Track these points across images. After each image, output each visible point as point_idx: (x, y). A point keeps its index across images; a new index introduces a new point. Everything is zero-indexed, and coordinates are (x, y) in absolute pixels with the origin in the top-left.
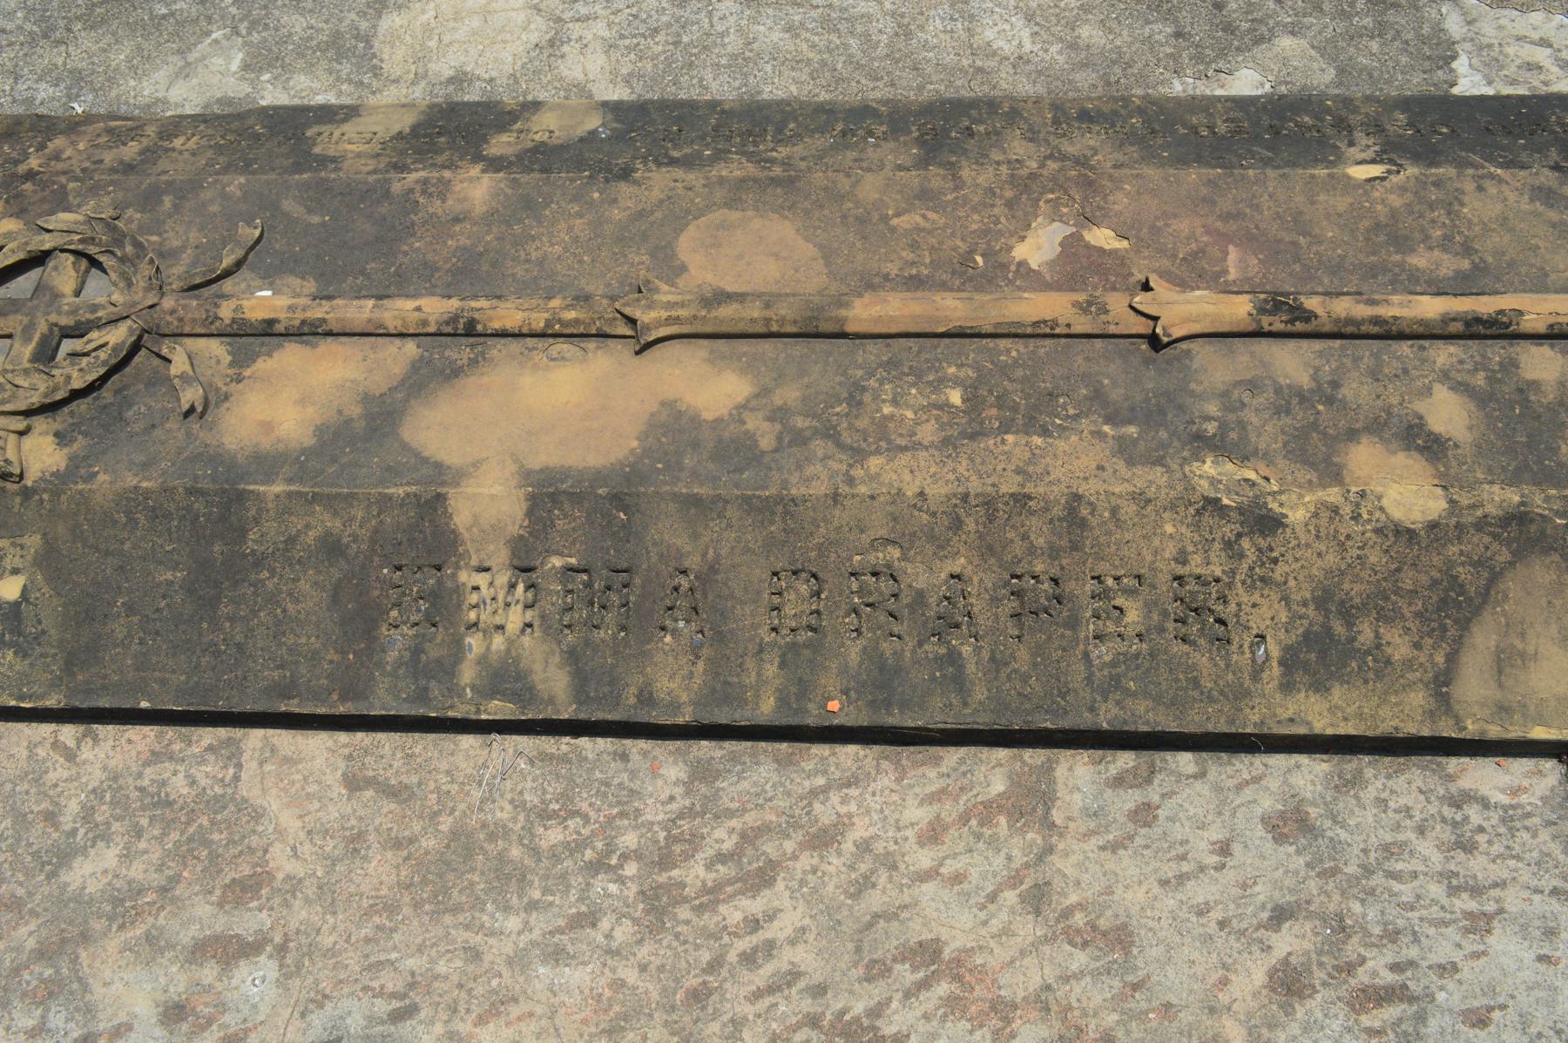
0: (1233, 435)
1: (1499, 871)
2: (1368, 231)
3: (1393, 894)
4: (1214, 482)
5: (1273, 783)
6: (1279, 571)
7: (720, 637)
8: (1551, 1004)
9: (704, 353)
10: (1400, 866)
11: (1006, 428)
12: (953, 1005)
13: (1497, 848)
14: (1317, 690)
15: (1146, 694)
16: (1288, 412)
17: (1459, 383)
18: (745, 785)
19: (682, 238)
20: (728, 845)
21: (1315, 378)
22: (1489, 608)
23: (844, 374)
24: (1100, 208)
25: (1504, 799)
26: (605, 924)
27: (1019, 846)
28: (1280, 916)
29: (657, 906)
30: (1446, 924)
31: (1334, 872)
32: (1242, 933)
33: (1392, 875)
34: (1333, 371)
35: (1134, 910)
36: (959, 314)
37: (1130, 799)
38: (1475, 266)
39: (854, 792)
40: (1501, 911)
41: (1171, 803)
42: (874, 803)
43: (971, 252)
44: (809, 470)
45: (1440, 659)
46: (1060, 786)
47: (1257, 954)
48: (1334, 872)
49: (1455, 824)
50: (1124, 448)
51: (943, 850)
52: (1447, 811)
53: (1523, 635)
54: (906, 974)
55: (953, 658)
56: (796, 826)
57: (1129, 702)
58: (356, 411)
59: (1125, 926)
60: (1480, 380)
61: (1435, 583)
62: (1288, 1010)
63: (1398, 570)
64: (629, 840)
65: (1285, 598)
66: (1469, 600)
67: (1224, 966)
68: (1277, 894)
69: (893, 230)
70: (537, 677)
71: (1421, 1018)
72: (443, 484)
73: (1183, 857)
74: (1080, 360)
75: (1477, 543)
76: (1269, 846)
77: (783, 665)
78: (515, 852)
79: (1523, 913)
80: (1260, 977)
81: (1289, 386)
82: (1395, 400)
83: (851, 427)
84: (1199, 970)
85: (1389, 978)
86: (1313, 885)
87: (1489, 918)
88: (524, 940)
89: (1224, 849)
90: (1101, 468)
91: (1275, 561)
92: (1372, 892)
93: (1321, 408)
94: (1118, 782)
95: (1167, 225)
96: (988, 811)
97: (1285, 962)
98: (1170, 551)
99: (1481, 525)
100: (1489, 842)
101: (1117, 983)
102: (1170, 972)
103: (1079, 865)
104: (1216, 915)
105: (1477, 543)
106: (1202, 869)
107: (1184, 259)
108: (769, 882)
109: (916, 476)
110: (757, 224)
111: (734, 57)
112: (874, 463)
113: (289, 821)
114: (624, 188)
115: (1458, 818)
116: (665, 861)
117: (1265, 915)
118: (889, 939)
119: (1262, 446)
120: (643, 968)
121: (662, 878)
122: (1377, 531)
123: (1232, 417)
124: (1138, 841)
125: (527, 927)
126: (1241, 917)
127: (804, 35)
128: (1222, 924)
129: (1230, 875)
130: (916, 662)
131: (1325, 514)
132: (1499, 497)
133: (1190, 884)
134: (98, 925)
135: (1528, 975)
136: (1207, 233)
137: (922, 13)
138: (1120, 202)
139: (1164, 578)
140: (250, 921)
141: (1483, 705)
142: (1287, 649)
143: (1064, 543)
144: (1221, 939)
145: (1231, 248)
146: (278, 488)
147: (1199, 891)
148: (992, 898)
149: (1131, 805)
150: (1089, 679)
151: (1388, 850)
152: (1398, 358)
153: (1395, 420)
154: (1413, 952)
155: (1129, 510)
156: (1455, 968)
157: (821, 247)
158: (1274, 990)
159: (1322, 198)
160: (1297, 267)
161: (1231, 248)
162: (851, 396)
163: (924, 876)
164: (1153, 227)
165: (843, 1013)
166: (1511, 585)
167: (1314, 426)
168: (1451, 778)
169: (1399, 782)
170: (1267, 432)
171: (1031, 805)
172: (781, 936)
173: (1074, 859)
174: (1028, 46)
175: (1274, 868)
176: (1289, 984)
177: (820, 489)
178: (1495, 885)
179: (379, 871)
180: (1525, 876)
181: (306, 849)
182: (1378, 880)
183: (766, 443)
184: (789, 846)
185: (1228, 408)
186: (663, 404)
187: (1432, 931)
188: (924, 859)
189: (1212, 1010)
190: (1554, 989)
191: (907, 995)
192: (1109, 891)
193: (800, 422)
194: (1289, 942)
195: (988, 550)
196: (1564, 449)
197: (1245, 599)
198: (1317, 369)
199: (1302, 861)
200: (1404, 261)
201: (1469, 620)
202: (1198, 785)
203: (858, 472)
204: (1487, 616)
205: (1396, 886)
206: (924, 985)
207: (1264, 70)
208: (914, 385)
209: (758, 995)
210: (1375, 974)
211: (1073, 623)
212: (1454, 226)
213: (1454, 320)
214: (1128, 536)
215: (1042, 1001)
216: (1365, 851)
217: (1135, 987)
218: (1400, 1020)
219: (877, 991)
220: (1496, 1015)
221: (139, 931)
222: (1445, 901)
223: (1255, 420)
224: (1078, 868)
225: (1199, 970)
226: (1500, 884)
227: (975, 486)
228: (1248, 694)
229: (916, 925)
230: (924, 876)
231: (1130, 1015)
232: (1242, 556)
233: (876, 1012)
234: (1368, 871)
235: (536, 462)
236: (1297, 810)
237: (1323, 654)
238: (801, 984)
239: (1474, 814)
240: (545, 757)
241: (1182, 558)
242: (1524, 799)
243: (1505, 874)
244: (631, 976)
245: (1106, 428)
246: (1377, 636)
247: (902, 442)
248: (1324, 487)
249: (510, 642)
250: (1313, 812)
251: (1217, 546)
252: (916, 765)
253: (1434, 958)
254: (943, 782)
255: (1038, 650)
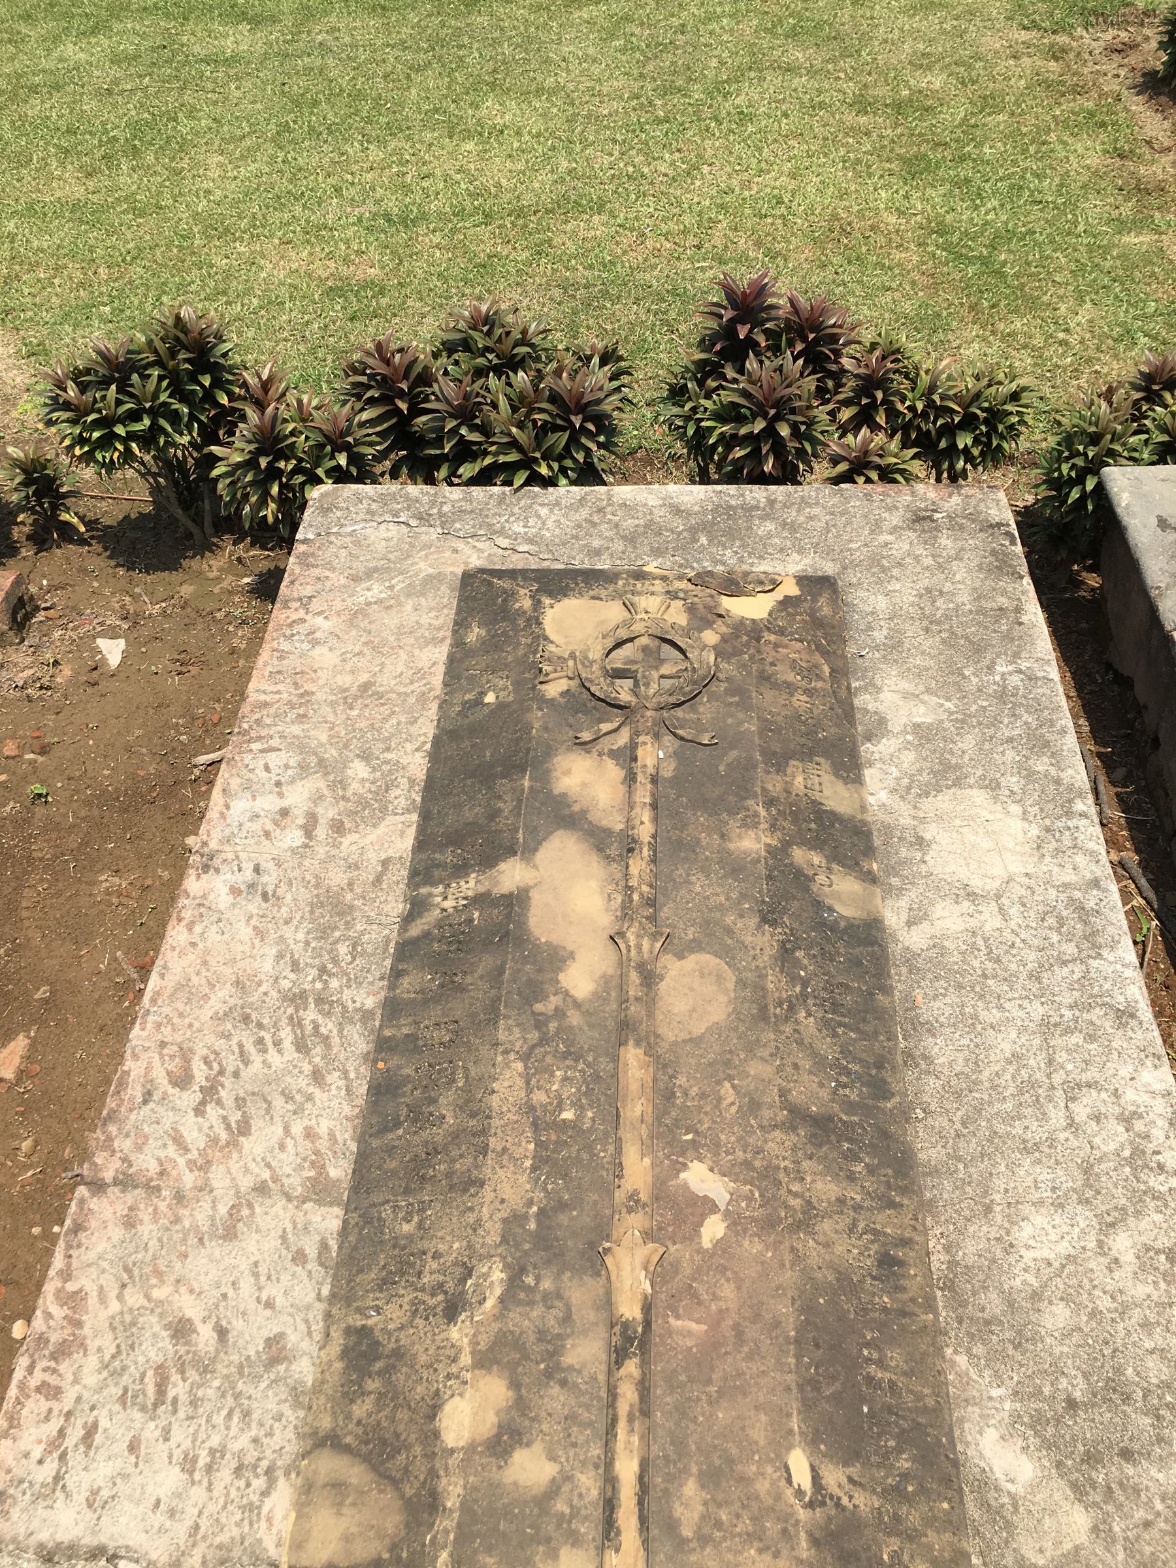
0: (522, 1295)
1: (218, 1490)
2: (725, 1450)
3: (219, 1409)
4: (486, 1276)
5: (305, 1345)
6: (420, 1322)
7: (426, 1002)
8: (130, 1498)
9: (610, 971)
10: (235, 1419)
11: (539, 1144)
12: (214, 1141)
13: (233, 1493)
14: (343, 1351)
15: (358, 1241)
16: (539, 1340)
17: (559, 1488)
18: (356, 1037)
19: (708, 956)
20: (323, 1030)
21: (571, 1368)
22: (376, 1478)
23: (590, 1050)
24: (745, 1231)
25: (265, 1510)
26: (292, 976)
27: (295, 1184)
28: (222, 1333)
29: (298, 999)
30: (193, 1442)
31: (241, 1373)
32: (217, 1307)
33: (230, 1415)
34: (575, 1385)
35: (243, 1244)
36: (629, 1114)
37: (312, 1251)
38: (684, 1541)
39: (343, 1092)
40: (193, 1483)
41: (304, 1275)
42: (334, 1104)
43: (697, 1132)
44: (516, 1030)
45: (348, 1439)
46: (327, 1209)
47: (203, 1314)
48: (241, 1373)
49: (255, 1467)
50: (517, 1219)
51: (300, 1140)
52: (264, 1464)
53: (354, 1504)
54: (235, 1117)
55: (398, 1124)
56: (327, 1064)
57: (356, 1231)
58: (576, 808)
59: (236, 1237)
60: (561, 1506)
61: (397, 1436)
62: (167, 1327)
63: (410, 1408)
64: (334, 983)
65: (402, 1328)
66: (383, 1462)
67: (200, 1293)
68: (235, 1333)
69: (719, 1083)
70: (419, 921)
71: (143, 1409)
72: (523, 853)
73: (269, 1278)
74: (595, 1197)
75: (420, 1470)
76: (266, 1334)
77: (407, 1036)
78: (337, 934)
79: (189, 1498)
80: (189, 1313)
81: (563, 1346)
82: (545, 1427)
83: (547, 1053)
84: (202, 1278)
85: (171, 1394)
86: (235, 1358)
87: (191, 1473)
88: (291, 942)
89: (269, 1305)
90: (503, 1201)
91: (427, 1319)
92: (223, 1396)
93: (542, 1366)
94: (324, 1246)
95: (728, 1280)
96: (319, 1166)
97: (195, 1331)
98: (442, 1247)
99: (433, 1474)
100: (238, 1489)
101: (205, 1229)
102: (205, 1261)
103: (277, 1216)
104: (231, 1294)
105: (420, 1470)
106: (260, 1289)
107: (691, 1286)
108: (298, 1050)
109: (508, 1086)
110: (723, 999)
111: (975, 1017)
112: (519, 1066)
113: (372, 837)
114: (754, 921)
115: (259, 1470)
116: (320, 1001)
117: (224, 1323)
118: (255, 1109)
119: (512, 1315)
120: (266, 994)
121: (311, 1000)
122: (438, 1390)
123: (538, 1297)
124: (284, 1252)
125: (296, 942)
126: (226, 1308)
127: (1011, 1069)
128: (224, 1296)
129: (252, 1305)
130: (398, 1104)
131: (452, 1353)
132: (453, 1492)
133: (252, 1279)
134: (331, 778)
135: (150, 1489)
136: (720, 1311)
137: (1057, 1163)
138: (752, 1247)
139: (426, 1244)
140: (321, 832)
141: (315, 1472)
142: (371, 1330)
143: (455, 1180)
144: (217, 1293)
145: (704, 1327)
146: (527, 784)
147: (247, 1284)
148: (268, 1165)
149: (307, 1251)
150: (374, 1205)
151: (247, 1414)
152: (587, 1442)
153: (527, 1423)
154: (181, 1414)
155: (471, 1218)
156: (167, 1439)
157: (701, 1038)
158: (180, 1321)
159: (763, 1418)
160: (683, 1378)
161: (704, 1327)
162: (570, 1054)
163: (287, 1129)
164: (725, 1268)
165: (223, 1086)
166: (389, 1495)
167: (526, 1357)
168: (287, 1474)
169: (290, 1434)
170: (525, 1321)
171: (319, 1190)
172: (268, 1056)
173: (281, 1212)
174: (1028, 1255)
175: (251, 1335)
176: (181, 1330)
177: (502, 1036)
178: (210, 1484)
179: (337, 877)
180: (212, 1508)
181: (354, 847)
182: (230, 1401)
183: (538, 1007)
184: (317, 1060)
185: (546, 1296)
186: (572, 953)
187: (191, 1430)
188: (297, 1129)
189: (178, 1281)
190: (138, 1503)
191: (225, 1118)
192: (258, 1231)
193: (553, 1026)
194: (205, 1336)
195: (456, 1136)
196: (490, 1560)
197: (406, 1299)
198: (579, 1372)
199: (252, 1353)
200: (691, 1475)
201: (370, 1462)
202: (313, 1295)
203: (512, 1056)
204: (370, 1476)
205: (224, 1413)
206: (228, 1127)
207: (1034, 1487)
208: (579, 1090)
209: (241, 1046)
210: (175, 1385)
211: (407, 1191)
212: (733, 1536)
213: (614, 1488)
214: (454, 1219)
215: (205, 1188)
216: (250, 1397)
217: (201, 1240)
218: (145, 1395)
219: (229, 1101)
220: (133, 1459)
221: (326, 792)
222: (207, 1445)
223: (534, 1314)
224: (275, 1215)
225: (202, 1278)
226: (209, 1489)
227: (496, 1122)
228: (349, 1306)
229: (261, 1123)
230: (287, 1129)
231: (186, 1233)
232: (433, 1295)
233: (219, 1102)
234: (237, 1396)
235: (535, 895)
236: (285, 1358)
237: (363, 1355)
238: (241, 1066)
239: (259, 1483)
240: (387, 943)
241: (436, 1256)
242: (263, 1524)
243: (216, 1493)
244: (263, 989)
245: (535, 1209)
246: (370, 1393)
247: (533, 1082)
248: (473, 1353)
249: (437, 905)
250: (281, 1368)
251: (441, 1278)
252: (355, 1129)
253: (175, 1427)
254: (340, 1139)
255: (394, 1173)
